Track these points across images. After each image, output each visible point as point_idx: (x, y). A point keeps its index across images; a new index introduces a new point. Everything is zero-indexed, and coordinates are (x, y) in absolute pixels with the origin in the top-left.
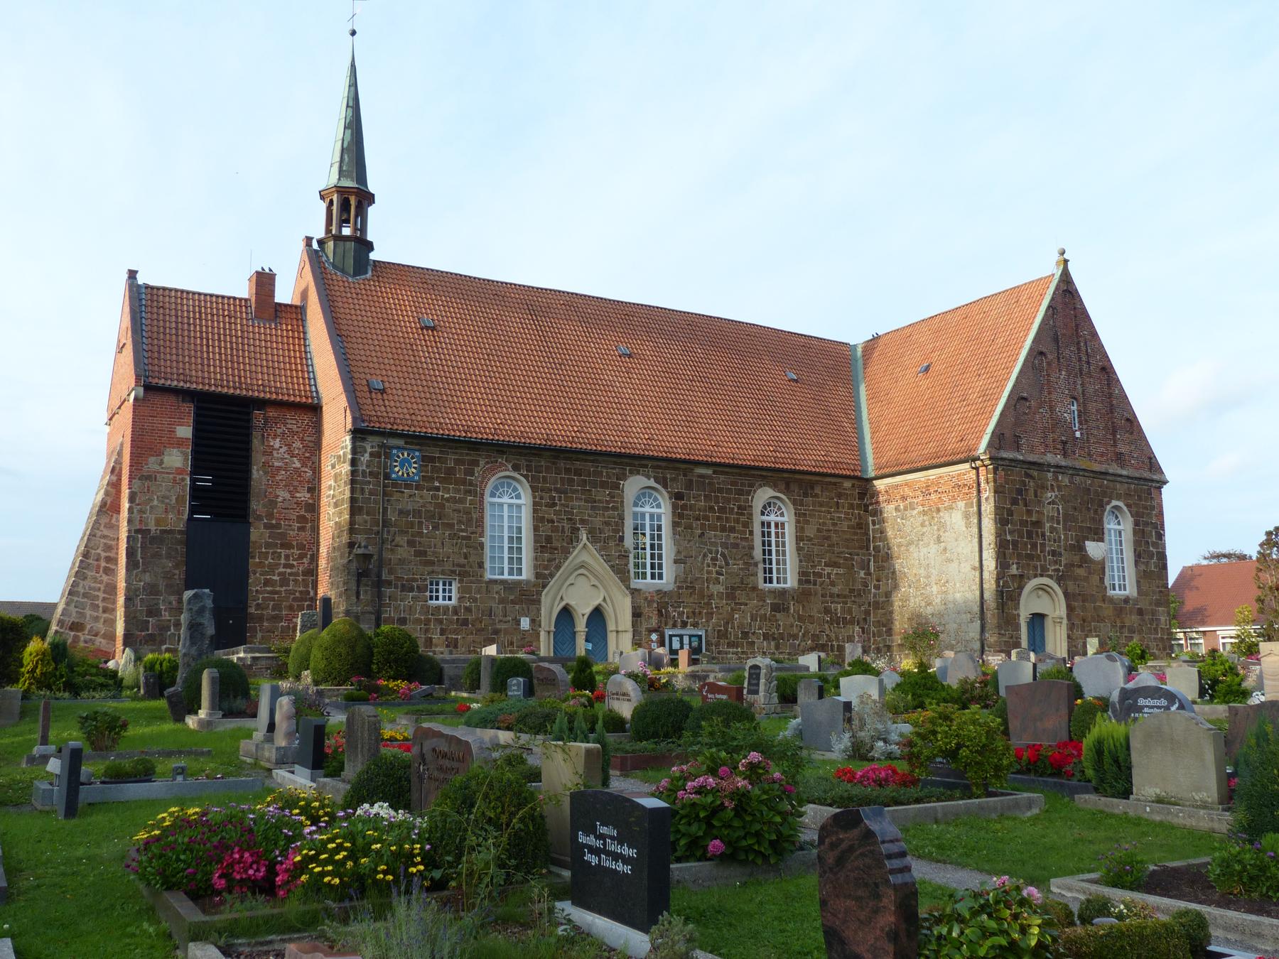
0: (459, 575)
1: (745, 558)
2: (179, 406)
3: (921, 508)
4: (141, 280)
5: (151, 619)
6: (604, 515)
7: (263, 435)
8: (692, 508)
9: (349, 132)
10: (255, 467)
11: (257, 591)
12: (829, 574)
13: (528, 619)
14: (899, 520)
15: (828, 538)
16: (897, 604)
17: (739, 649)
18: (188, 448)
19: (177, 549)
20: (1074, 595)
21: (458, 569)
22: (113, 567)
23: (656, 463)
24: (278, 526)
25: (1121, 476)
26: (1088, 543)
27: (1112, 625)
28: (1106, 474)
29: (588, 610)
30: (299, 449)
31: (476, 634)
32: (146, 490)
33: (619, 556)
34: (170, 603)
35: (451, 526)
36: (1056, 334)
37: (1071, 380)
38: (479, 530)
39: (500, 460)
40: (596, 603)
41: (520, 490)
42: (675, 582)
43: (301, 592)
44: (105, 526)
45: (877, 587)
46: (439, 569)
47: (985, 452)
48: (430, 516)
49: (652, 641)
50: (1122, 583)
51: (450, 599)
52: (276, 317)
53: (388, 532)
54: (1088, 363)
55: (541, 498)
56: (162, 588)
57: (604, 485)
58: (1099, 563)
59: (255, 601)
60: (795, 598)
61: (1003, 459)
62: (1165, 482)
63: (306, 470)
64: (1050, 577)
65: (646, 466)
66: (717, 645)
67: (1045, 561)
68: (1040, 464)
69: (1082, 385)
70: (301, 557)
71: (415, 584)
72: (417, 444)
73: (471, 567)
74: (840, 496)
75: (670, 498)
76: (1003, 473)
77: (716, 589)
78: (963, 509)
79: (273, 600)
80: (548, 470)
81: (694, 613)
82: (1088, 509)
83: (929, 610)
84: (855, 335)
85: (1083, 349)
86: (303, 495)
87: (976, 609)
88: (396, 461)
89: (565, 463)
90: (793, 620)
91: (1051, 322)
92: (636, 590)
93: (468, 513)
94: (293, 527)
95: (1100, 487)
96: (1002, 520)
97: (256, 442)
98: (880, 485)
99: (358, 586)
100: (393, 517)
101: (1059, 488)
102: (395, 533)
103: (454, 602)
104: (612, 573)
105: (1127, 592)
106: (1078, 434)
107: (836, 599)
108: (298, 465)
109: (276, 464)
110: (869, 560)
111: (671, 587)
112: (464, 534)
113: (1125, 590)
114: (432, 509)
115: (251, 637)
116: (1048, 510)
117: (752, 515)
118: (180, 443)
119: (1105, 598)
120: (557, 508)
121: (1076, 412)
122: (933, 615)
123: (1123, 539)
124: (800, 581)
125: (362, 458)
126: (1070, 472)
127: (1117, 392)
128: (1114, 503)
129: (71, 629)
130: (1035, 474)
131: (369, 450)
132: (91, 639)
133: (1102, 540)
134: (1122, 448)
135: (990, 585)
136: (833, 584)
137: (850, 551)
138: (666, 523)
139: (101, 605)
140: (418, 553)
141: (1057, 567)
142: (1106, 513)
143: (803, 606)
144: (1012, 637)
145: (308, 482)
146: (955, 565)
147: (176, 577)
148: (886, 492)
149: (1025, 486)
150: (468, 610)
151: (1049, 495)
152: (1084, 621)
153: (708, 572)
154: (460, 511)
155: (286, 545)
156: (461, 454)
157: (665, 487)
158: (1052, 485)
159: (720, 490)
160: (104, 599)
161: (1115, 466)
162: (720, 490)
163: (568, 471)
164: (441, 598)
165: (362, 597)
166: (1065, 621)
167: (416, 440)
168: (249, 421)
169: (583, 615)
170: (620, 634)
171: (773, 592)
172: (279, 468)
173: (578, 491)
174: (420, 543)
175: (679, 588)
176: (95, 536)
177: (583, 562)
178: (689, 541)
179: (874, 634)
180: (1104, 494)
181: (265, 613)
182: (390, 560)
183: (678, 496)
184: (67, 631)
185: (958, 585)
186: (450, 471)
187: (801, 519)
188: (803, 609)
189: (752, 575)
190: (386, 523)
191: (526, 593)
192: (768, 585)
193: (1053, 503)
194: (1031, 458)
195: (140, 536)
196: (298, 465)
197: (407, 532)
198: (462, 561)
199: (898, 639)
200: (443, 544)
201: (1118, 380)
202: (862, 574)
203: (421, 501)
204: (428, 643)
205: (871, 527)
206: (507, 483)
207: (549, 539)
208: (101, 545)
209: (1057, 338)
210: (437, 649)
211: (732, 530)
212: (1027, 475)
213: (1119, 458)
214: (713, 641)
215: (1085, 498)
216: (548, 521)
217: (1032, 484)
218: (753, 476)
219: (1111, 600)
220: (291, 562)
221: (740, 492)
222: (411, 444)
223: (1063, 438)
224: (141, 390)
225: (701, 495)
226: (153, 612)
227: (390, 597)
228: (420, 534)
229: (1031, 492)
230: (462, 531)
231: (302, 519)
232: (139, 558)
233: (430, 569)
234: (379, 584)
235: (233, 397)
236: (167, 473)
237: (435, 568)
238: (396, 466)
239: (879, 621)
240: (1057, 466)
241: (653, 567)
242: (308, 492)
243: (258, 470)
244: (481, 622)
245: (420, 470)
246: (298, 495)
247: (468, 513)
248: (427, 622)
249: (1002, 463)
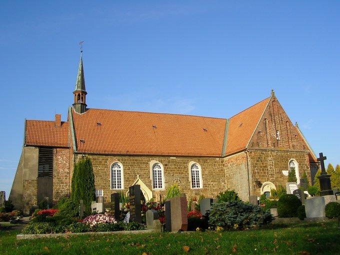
57: (144, 163)
84: (227, 116)
101: (273, 156)
124: (204, 187)
136: (214, 187)
155: (63, 183)
183: (166, 165)
192: (194, 188)
211: (182, 173)
231: (66, 176)
241: (159, 179)
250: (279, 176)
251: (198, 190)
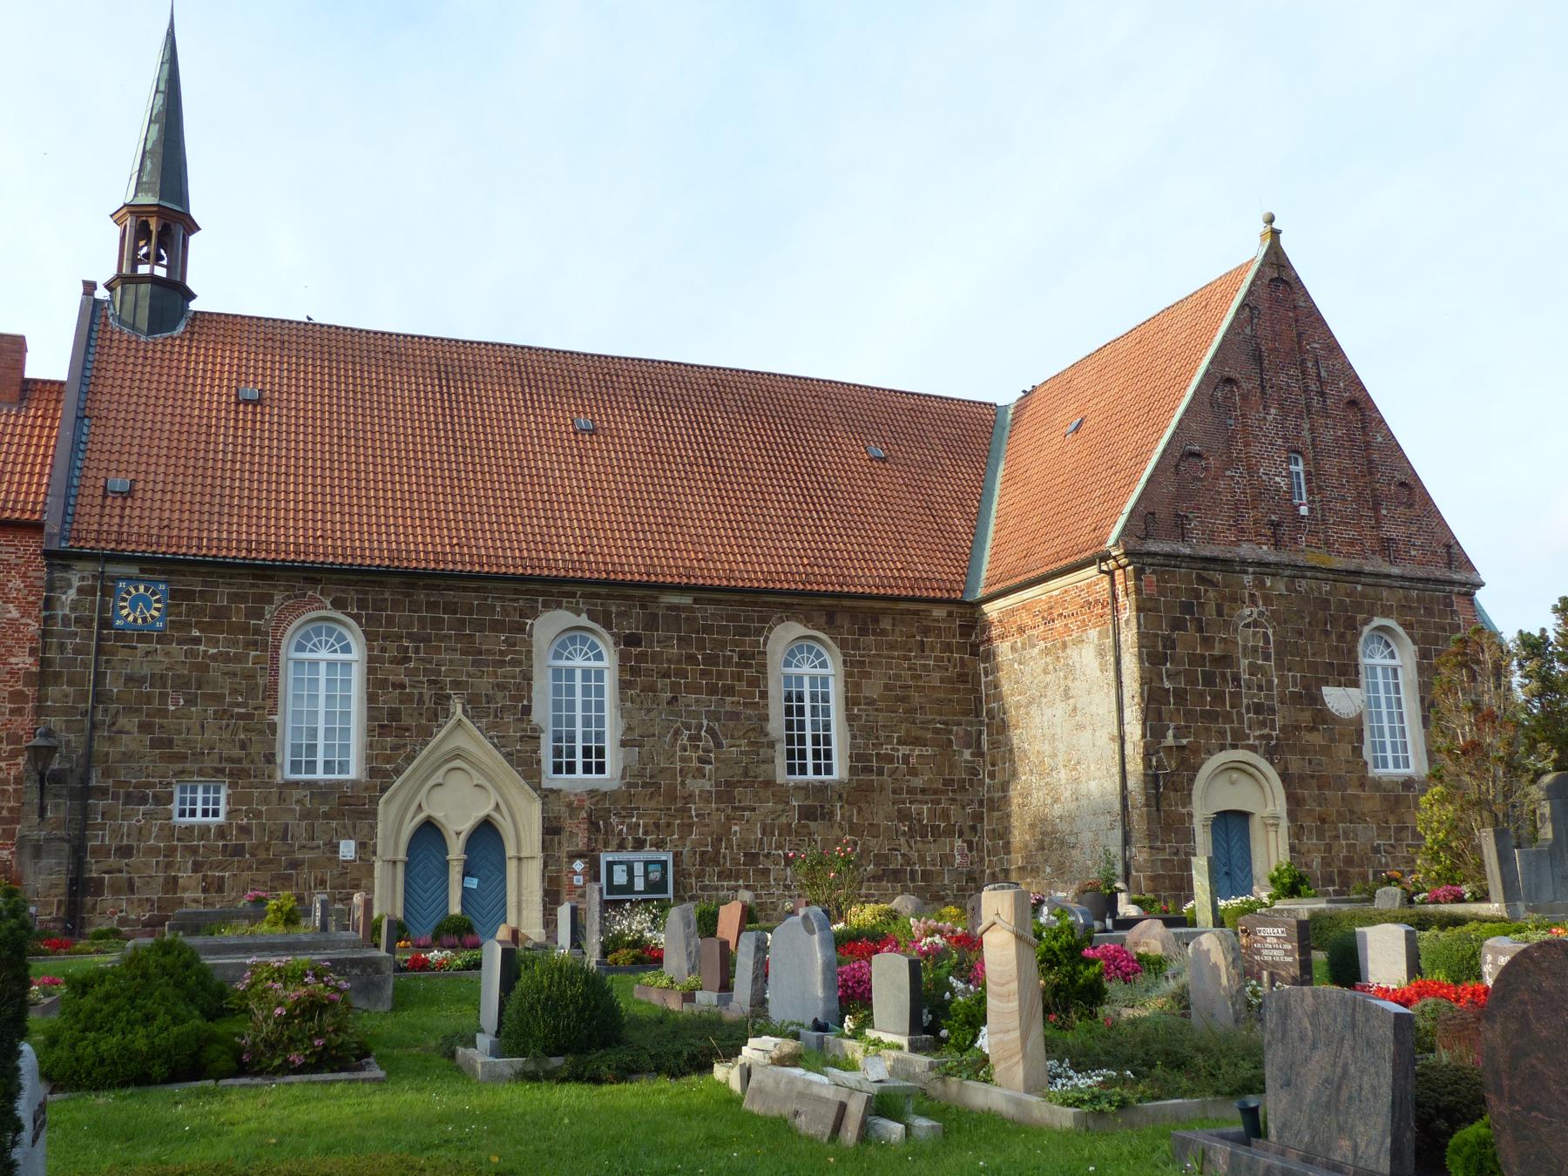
0: (231, 775)
1: (751, 734)
3: (1042, 644)
6: (495, 673)
8: (655, 658)
9: (155, 128)
12: (906, 758)
13: (352, 843)
14: (1016, 666)
15: (903, 699)
16: (1016, 800)
17: (741, 882)
20: (1301, 777)
21: (228, 766)
23: (588, 590)
25: (1388, 576)
26: (1325, 690)
27: (1379, 827)
28: (1358, 573)
29: (467, 826)
30: (19, 590)
31: (257, 869)
33: (522, 737)
36: (1258, 349)
37: (1290, 423)
38: (270, 702)
39: (310, 593)
40: (482, 813)
41: (826, 656)
42: (623, 777)
43: (11, 810)
45: (992, 776)
46: (196, 767)
47: (1116, 544)
48: (182, 684)
49: (575, 873)
51: (216, 813)
52: (22, 400)
53: (106, 711)
54: (1322, 394)
55: (383, 650)
57: (497, 626)
58: (1350, 722)
60: (845, 796)
61: (1149, 554)
62: (1480, 585)
63: (29, 621)
64: (1253, 748)
65: (573, 595)
66: (700, 875)
67: (1241, 721)
68: (1225, 561)
69: (1312, 430)
71: (150, 792)
72: (163, 573)
73: (252, 762)
74: (926, 631)
75: (616, 644)
76: (1154, 578)
77: (696, 786)
78: (1096, 641)
80: (396, 605)
81: (657, 825)
82: (1327, 633)
83: (1058, 810)
84: (1004, 394)
85: (1312, 371)
87: (1117, 807)
88: (124, 600)
89: (427, 595)
90: (840, 833)
91: (1248, 330)
92: (551, 791)
93: (250, 676)
95: (1348, 595)
96: (1153, 655)
98: (992, 610)
100: (113, 686)
101: (1267, 600)
102: (118, 712)
103: (221, 818)
104: (506, 764)
105: (1410, 771)
106: (1304, 511)
107: (919, 797)
108: (15, 614)
110: (980, 733)
111: (615, 785)
112: (243, 710)
116: (1245, 638)
117: (765, 666)
119: (1363, 782)
120: (412, 665)
121: (1302, 475)
122: (1061, 818)
123: (1401, 681)
124: (853, 770)
125: (64, 597)
126: (1288, 572)
127: (1380, 439)
128: (1378, 621)
130: (1219, 577)
131: (76, 583)
133: (1356, 684)
134: (1392, 530)
135: (1135, 766)
136: (913, 772)
137: (944, 718)
138: (835, 691)
140: (155, 744)
141: (1266, 731)
142: (1362, 640)
143: (860, 810)
144: (1176, 853)
146: (1087, 734)
148: (1000, 621)
149: (1198, 597)
150: (245, 830)
151: (1247, 611)
152: (1323, 821)
153: (683, 760)
154: (235, 675)
156: (242, 585)
157: (608, 626)
158: (1252, 595)
159: (707, 629)
161: (1378, 559)
162: (707, 629)
163: (432, 606)
164: (199, 812)
165: (49, 815)
166: (1284, 823)
167: (155, 565)
169: (458, 834)
170: (525, 864)
171: (805, 788)
173: (450, 637)
174: (161, 726)
175: (629, 785)
177: (458, 748)
178: (649, 711)
179: (989, 852)
180: (1358, 607)
182: (107, 754)
183: (631, 641)
185: (1092, 768)
186: (220, 613)
187: (855, 671)
188: (858, 813)
189: (764, 762)
190: (99, 697)
191: (351, 801)
192: (798, 777)
193: (1256, 624)
194: (1207, 551)
196: (15, 614)
197: (139, 710)
198: (237, 752)
199: (1017, 859)
200: (203, 727)
201: (1382, 421)
202: (967, 755)
203: (167, 660)
204: (171, 886)
205: (983, 679)
206: (593, 643)
207: (394, 714)
209: (1260, 356)
210: (186, 895)
211: (730, 691)
212: (1202, 580)
213: (1386, 547)
214: (693, 870)
215: (1320, 614)
216: (394, 686)
217: (1211, 594)
218: (767, 604)
219: (1377, 784)
221: (745, 632)
222: (153, 572)
223: (1273, 517)
225: (673, 637)
227: (103, 814)
228: (164, 713)
229: (1211, 609)
230: (239, 705)
233: (178, 766)
234: (85, 793)
237: (188, 766)
238: (123, 608)
239: (994, 830)
240: (1260, 564)
241: (816, 754)
244: (268, 849)
245: (167, 611)
246: (13, 660)
247: (250, 676)
248: (171, 851)
249: (1150, 561)
250: (1306, 717)
251: (823, 787)
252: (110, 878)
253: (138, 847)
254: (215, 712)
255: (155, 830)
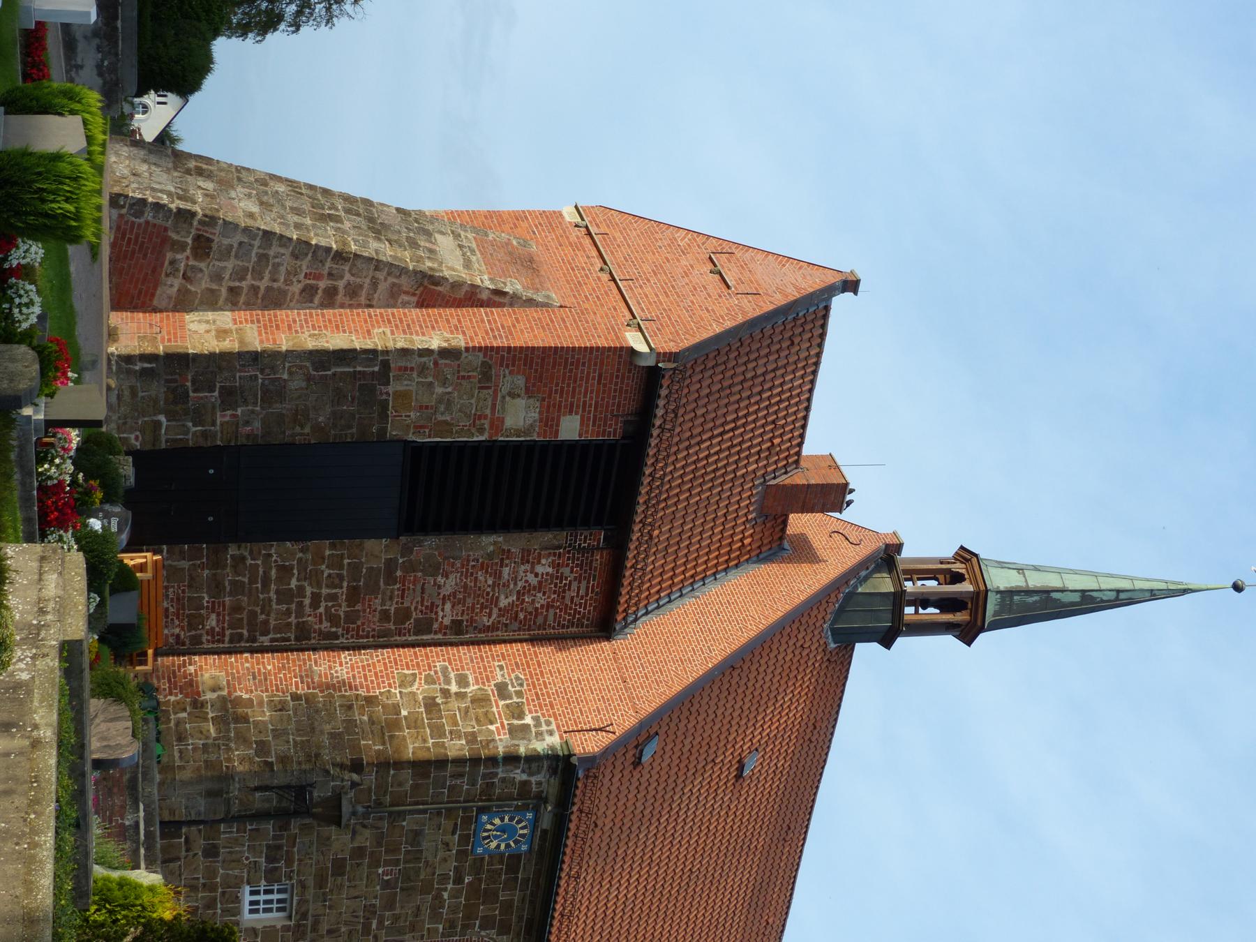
0: (298, 926)
2: (617, 416)
4: (841, 304)
5: (216, 394)
7: (559, 547)
10: (501, 539)
11: (270, 555)
18: (539, 434)
19: (350, 427)
21: (309, 922)
22: (317, 300)
24: (390, 579)
32: (462, 374)
34: (247, 423)
35: (390, 905)
44: (394, 285)
50: (262, 906)
56: (277, 408)
59: (251, 553)
63: (494, 616)
70: (333, 619)
72: (541, 847)
79: (253, 580)
86: (447, 614)
88: (511, 819)
94: (388, 603)
97: (547, 537)
99: (280, 788)
102: (378, 828)
108: (503, 602)
109: (506, 571)
112: (374, 926)
113: (251, 911)
114: (422, 877)
115: (182, 552)
118: (550, 421)
129: (198, 238)
131: (533, 779)
132: (177, 270)
139: (244, 284)
145: (472, 620)
147: (298, 429)
155: (354, 595)
160: (255, 289)
165: (258, 795)
168: (586, 524)
172: (497, 575)
174: (358, 865)
176: (377, 268)
181: (228, 570)
184: (193, 232)
195: (376, 369)
197: (379, 844)
198: (324, 927)
208: (358, 280)
220: (323, 604)
224: (651, 362)
226: (230, 397)
227: (257, 830)
230: (380, 923)
231: (404, 615)
232: (333, 370)
233: (311, 882)
235: (631, 511)
236: (494, 405)
238: (502, 819)
242: (453, 621)
243: (495, 543)
245: (497, 856)
246: (448, 606)
248: (211, 888)
252: (180, 843)
253: (218, 862)
254: (374, 906)
255: (236, 872)
